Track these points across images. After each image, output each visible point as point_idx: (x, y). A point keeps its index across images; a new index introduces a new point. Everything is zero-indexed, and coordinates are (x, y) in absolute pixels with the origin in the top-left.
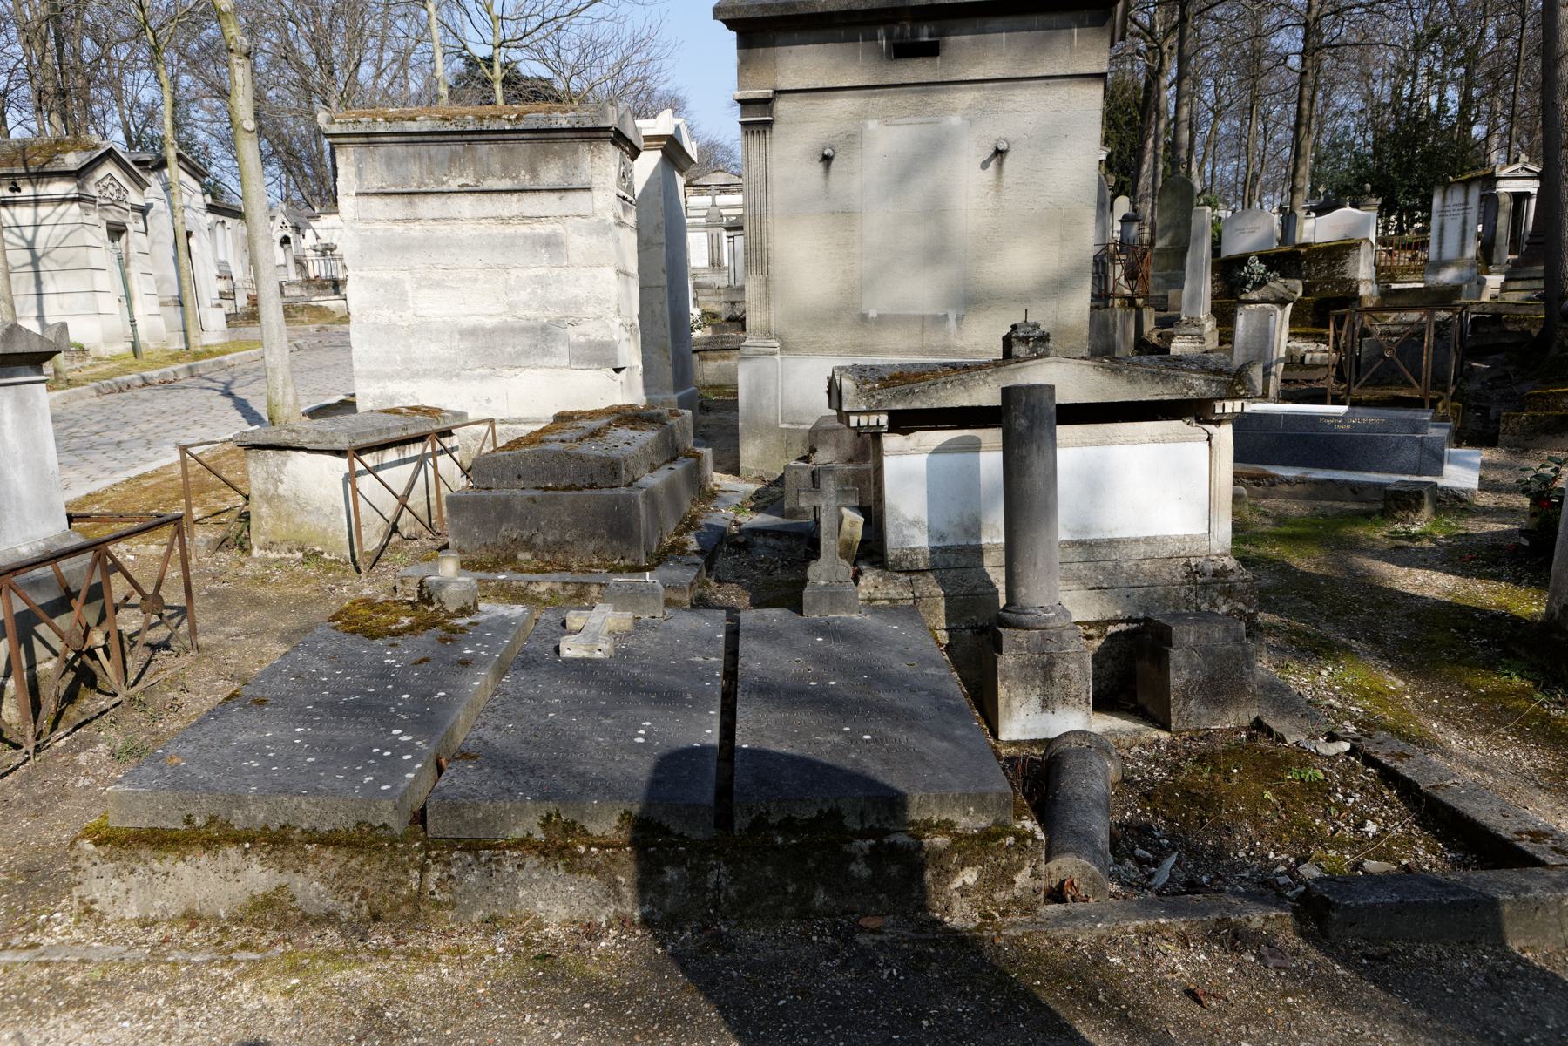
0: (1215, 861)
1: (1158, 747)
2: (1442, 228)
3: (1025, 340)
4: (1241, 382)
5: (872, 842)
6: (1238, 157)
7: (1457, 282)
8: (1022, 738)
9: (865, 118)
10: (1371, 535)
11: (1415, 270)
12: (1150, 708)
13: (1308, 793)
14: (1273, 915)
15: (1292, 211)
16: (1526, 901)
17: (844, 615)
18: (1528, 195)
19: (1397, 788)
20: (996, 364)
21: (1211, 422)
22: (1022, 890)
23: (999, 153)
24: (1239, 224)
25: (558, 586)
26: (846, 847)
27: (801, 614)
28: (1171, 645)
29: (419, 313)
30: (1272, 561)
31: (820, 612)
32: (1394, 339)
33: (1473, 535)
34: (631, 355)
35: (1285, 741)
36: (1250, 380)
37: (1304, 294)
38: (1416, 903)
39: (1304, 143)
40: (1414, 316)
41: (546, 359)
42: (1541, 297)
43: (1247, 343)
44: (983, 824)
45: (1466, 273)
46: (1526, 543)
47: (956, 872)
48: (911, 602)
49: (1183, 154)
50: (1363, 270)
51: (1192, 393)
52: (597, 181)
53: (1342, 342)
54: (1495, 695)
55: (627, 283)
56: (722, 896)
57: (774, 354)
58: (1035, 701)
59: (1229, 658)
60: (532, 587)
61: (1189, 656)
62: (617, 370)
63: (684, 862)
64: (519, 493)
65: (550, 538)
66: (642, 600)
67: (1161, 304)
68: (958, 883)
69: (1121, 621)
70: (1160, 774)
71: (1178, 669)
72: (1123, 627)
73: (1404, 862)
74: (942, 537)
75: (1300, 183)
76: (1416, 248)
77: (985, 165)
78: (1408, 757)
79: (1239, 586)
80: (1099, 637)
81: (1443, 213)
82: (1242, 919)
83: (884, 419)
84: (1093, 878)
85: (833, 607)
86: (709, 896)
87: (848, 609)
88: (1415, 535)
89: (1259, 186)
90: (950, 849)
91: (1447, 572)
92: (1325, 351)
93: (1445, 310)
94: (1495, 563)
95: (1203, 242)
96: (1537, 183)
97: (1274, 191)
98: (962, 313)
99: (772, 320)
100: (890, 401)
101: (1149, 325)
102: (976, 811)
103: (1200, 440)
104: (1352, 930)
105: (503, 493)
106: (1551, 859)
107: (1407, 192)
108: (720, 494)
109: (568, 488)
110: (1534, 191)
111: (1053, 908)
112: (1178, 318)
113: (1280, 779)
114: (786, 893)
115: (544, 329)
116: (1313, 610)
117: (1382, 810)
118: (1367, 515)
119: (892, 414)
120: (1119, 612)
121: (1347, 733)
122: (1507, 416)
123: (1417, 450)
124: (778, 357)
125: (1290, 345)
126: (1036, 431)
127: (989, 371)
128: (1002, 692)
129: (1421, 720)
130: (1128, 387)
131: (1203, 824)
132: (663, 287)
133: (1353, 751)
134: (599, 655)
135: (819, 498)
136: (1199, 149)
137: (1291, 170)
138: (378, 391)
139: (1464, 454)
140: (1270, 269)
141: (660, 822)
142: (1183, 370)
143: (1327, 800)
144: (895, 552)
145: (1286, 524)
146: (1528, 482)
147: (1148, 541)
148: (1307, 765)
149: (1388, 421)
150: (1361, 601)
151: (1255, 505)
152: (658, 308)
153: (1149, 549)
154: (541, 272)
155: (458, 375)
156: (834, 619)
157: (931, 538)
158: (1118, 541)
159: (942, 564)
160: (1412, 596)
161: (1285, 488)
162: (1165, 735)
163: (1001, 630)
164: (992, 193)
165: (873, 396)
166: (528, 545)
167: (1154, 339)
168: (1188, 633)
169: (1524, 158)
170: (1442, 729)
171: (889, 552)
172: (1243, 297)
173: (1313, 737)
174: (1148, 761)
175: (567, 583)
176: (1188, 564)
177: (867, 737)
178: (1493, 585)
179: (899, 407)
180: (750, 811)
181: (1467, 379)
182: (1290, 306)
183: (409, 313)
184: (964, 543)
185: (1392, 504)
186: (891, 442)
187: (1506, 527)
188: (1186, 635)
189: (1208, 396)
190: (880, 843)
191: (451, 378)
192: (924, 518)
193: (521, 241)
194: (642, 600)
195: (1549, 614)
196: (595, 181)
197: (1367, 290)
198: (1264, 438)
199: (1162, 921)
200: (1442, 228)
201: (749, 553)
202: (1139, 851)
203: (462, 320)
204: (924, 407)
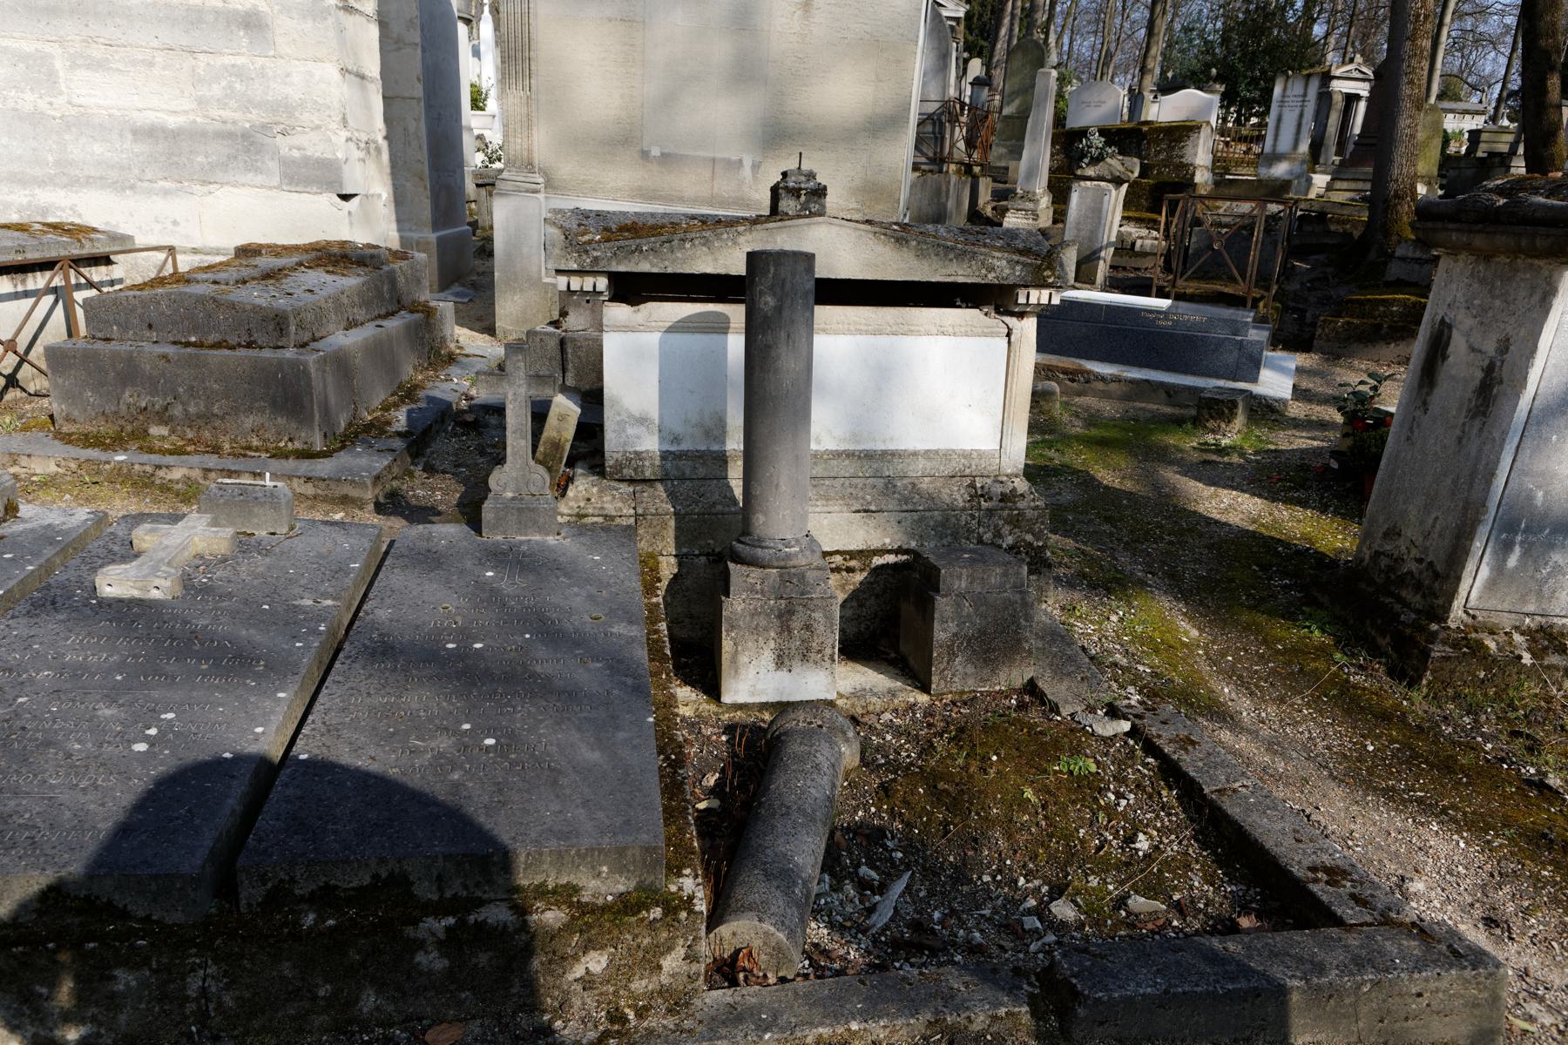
0: (953, 886)
1: (914, 714)
2: (1279, 120)
3: (795, 193)
4: (1050, 267)
5: (451, 920)
6: (1095, 33)
7: (1287, 177)
8: (750, 700)
10: (1182, 445)
11: (1249, 164)
12: (912, 661)
13: (1076, 791)
14: (1002, 1011)
15: (1140, 93)
16: (1319, 988)
17: (537, 538)
18: (1357, 97)
19: (1178, 787)
20: (756, 221)
21: (1012, 314)
22: (673, 976)
24: (1085, 96)
25: (196, 474)
26: (409, 931)
27: (481, 535)
28: (937, 591)
29: (76, 101)
30: (1076, 472)
31: (504, 533)
32: (1224, 230)
33: (1282, 452)
34: (375, 183)
35: (1058, 713)
36: (1062, 265)
37: (1141, 175)
38: (1184, 993)
39: (1158, 22)
40: (1245, 207)
41: (250, 176)
42: (1364, 199)
43: (1078, 223)
44: (621, 888)
45: (1297, 168)
46: (1334, 465)
47: (576, 958)
48: (632, 520)
49: (1041, 17)
50: (1201, 155)
51: (991, 276)
53: (1173, 229)
54: (1293, 652)
55: (363, 89)
56: (211, 1006)
57: (536, 192)
58: (768, 657)
59: (1007, 608)
60: (161, 473)
61: (958, 605)
62: (346, 197)
63: (146, 962)
64: (147, 347)
65: (192, 409)
66: (256, 510)
67: (1000, 175)
68: (579, 971)
69: (889, 552)
70: (909, 753)
73: (1176, 897)
74: (676, 439)
75: (1150, 64)
76: (1251, 142)
78: (1193, 743)
79: (1029, 514)
80: (862, 570)
81: (1282, 102)
82: (962, 1020)
83: (602, 283)
84: (778, 948)
85: (522, 528)
86: (190, 1007)
87: (543, 530)
88: (1224, 449)
89: (1112, 66)
90: (568, 928)
91: (1254, 494)
92: (1156, 239)
93: (1278, 203)
94: (1302, 486)
95: (1045, 108)
96: (1367, 86)
97: (1126, 73)
98: (758, 159)
99: (536, 149)
101: (985, 196)
102: (611, 871)
103: (997, 335)
104: (1101, 1029)
105: (125, 347)
106: (1349, 913)
107: (1249, 84)
108: (461, 358)
109: (217, 345)
110: (1365, 94)
111: (721, 997)
112: (1013, 191)
113: (1045, 771)
114: (315, 998)
115: (247, 137)
116: (1111, 534)
117: (1158, 816)
118: (1179, 422)
119: (614, 278)
120: (887, 541)
121: (1129, 706)
122: (1324, 321)
123: (1235, 354)
124: (541, 196)
125: (1122, 229)
126: (786, 313)
127: (741, 229)
128: (727, 645)
129: (1213, 684)
130: (914, 262)
131: (947, 832)
132: (419, 100)
133: (1134, 732)
134: (155, 594)
135: (505, 384)
136: (1059, 20)
137: (1143, 51)
138: (25, 200)
139: (1281, 359)
140: (1108, 143)
141: (110, 903)
142: (985, 245)
143: (1096, 800)
144: (615, 456)
145: (1095, 425)
146: (1345, 400)
147: (927, 454)
148: (1078, 753)
149: (1210, 319)
150: (1162, 527)
151: (1067, 403)
152: (412, 126)
153: (929, 465)
154: (240, 60)
155: (132, 187)
156: (522, 543)
157: (662, 439)
158: (893, 454)
159: (674, 472)
160: (1217, 522)
161: (1100, 386)
162: (923, 699)
163: (731, 566)
164: (799, 12)
165: (586, 252)
166: (163, 417)
167: (989, 212)
168: (960, 577)
169: (1359, 59)
170: (1234, 696)
171: (607, 455)
172: (1079, 172)
173: (1091, 709)
174: (898, 733)
175: (210, 470)
176: (972, 485)
177: (490, 741)
178: (1299, 512)
179: (622, 268)
180: (263, 880)
181: (1287, 279)
182: (1126, 185)
183: (60, 101)
184: (703, 448)
185: (1205, 412)
186: (618, 312)
187: (1315, 443)
188: (957, 579)
189: (1011, 281)
190: (462, 923)
191: (123, 189)
192: (654, 414)
193: (211, 18)
194: (256, 510)
195: (1359, 559)
197: (1202, 177)
198: (1084, 330)
199: (854, 1026)
200: (1279, 120)
201: (480, 434)
202: (864, 870)
203: (135, 114)
204: (655, 270)
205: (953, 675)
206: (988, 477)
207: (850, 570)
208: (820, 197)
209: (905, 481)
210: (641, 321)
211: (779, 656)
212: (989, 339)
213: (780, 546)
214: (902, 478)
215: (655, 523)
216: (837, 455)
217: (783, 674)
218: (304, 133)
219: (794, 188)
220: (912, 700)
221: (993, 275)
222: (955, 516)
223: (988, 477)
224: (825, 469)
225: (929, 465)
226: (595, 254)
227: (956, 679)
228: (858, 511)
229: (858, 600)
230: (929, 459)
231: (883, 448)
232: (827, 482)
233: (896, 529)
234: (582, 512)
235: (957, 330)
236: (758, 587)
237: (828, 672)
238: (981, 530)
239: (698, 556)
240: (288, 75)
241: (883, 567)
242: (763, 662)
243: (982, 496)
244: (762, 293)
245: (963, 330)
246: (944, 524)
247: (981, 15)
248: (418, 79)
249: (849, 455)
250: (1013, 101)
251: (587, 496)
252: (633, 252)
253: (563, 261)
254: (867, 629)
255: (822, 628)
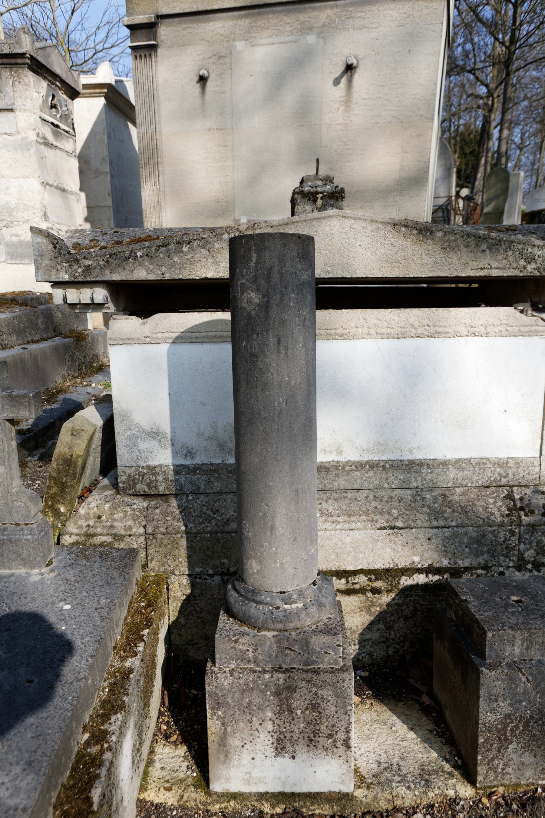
9: (234, 40)
23: (350, 68)
52: (18, 103)
61: (511, 680)
69: (419, 571)
71: (494, 699)
72: (420, 579)
74: (190, 453)
77: (337, 82)
80: (388, 591)
95: (517, 196)
100: (102, 268)
120: (417, 559)
126: (274, 312)
130: (440, 256)
132: (109, 207)
144: (128, 471)
147: (458, 463)
153: (461, 475)
157: (175, 453)
158: (421, 464)
159: (188, 487)
163: (223, 617)
164: (342, 108)
165: (77, 261)
168: (512, 642)
176: (510, 497)
179: (116, 277)
184: (218, 461)
192: (166, 427)
196: (17, 104)
204: (152, 277)
205: (506, 765)
206: (527, 486)
207: (376, 591)
208: (337, 200)
209: (436, 493)
210: (147, 333)
211: (278, 740)
212: (526, 339)
213: (278, 602)
214: (431, 489)
215: (165, 542)
216: (360, 466)
217: (285, 761)
218: (19, 225)
219: (309, 193)
220: (451, 793)
221: (533, 266)
222: (493, 532)
223: (527, 486)
224: (347, 481)
225: (461, 475)
226: (87, 263)
227: (510, 770)
228: (384, 528)
229: (385, 623)
230: (461, 468)
231: (410, 457)
232: (350, 495)
233: (426, 546)
234: (91, 531)
235: (489, 330)
236: (251, 655)
237: (341, 761)
238: (522, 547)
239: (212, 576)
240: (8, 189)
241: (412, 587)
242: (259, 747)
243: (522, 509)
244: (244, 288)
245: (496, 329)
246: (480, 540)
247: (466, 170)
248: (109, 194)
249: (373, 465)
250: (490, 204)
251: (98, 513)
252: (127, 259)
253: (54, 272)
254: (397, 652)
255: (333, 709)
